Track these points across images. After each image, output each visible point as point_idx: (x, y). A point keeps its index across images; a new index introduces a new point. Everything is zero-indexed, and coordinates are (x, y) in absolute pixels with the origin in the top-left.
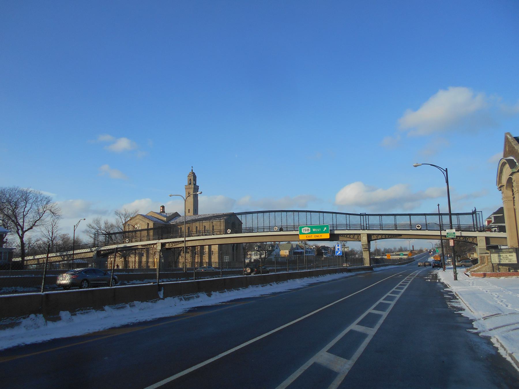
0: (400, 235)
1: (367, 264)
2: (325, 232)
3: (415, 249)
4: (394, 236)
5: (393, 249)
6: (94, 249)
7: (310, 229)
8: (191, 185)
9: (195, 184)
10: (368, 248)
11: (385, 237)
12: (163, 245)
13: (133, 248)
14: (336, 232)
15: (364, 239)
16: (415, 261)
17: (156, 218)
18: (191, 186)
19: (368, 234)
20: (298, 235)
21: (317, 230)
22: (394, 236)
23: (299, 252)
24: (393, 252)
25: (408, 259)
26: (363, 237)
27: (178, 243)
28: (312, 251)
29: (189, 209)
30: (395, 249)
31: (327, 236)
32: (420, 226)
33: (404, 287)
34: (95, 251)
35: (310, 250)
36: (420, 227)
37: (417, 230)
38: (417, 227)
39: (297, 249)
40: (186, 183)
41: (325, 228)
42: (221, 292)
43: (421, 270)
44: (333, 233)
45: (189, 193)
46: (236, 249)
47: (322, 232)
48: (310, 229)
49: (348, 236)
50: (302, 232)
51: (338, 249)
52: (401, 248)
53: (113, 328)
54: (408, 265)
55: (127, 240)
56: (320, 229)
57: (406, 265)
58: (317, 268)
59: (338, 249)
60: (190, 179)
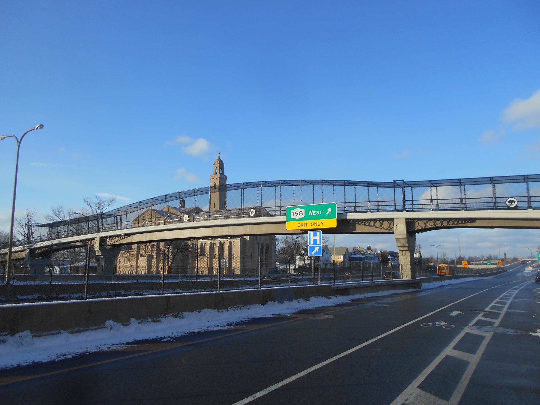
0: (473, 220)
1: (406, 275)
2: (330, 217)
3: (507, 257)
4: (460, 222)
5: (480, 257)
6: (26, 246)
7: (303, 211)
8: (216, 175)
9: (222, 174)
10: (407, 246)
11: (442, 224)
12: (103, 240)
13: (70, 245)
14: (350, 216)
15: (401, 228)
16: (507, 272)
17: (171, 213)
18: (217, 176)
19: (407, 219)
20: (284, 222)
21: (316, 213)
22: (463, 222)
23: (357, 258)
24: (480, 261)
25: (498, 268)
26: (398, 225)
27: (119, 238)
28: (375, 257)
29: (214, 204)
30: (483, 257)
31: (332, 223)
32: (514, 202)
33: (489, 309)
34: (27, 249)
35: (373, 256)
36: (516, 203)
37: (509, 208)
38: (507, 203)
39: (355, 254)
40: (212, 172)
41: (330, 210)
42: (35, 336)
43: (516, 289)
44: (344, 218)
45: (214, 184)
46: (267, 253)
47: (324, 216)
48: (303, 211)
49: (372, 223)
50: (292, 216)
51: (315, 241)
52: (490, 255)
53: (319, 307)
54: (496, 277)
55: (63, 234)
56: (321, 211)
57: (494, 276)
58: (264, 286)
59: (315, 241)
60: (216, 168)
